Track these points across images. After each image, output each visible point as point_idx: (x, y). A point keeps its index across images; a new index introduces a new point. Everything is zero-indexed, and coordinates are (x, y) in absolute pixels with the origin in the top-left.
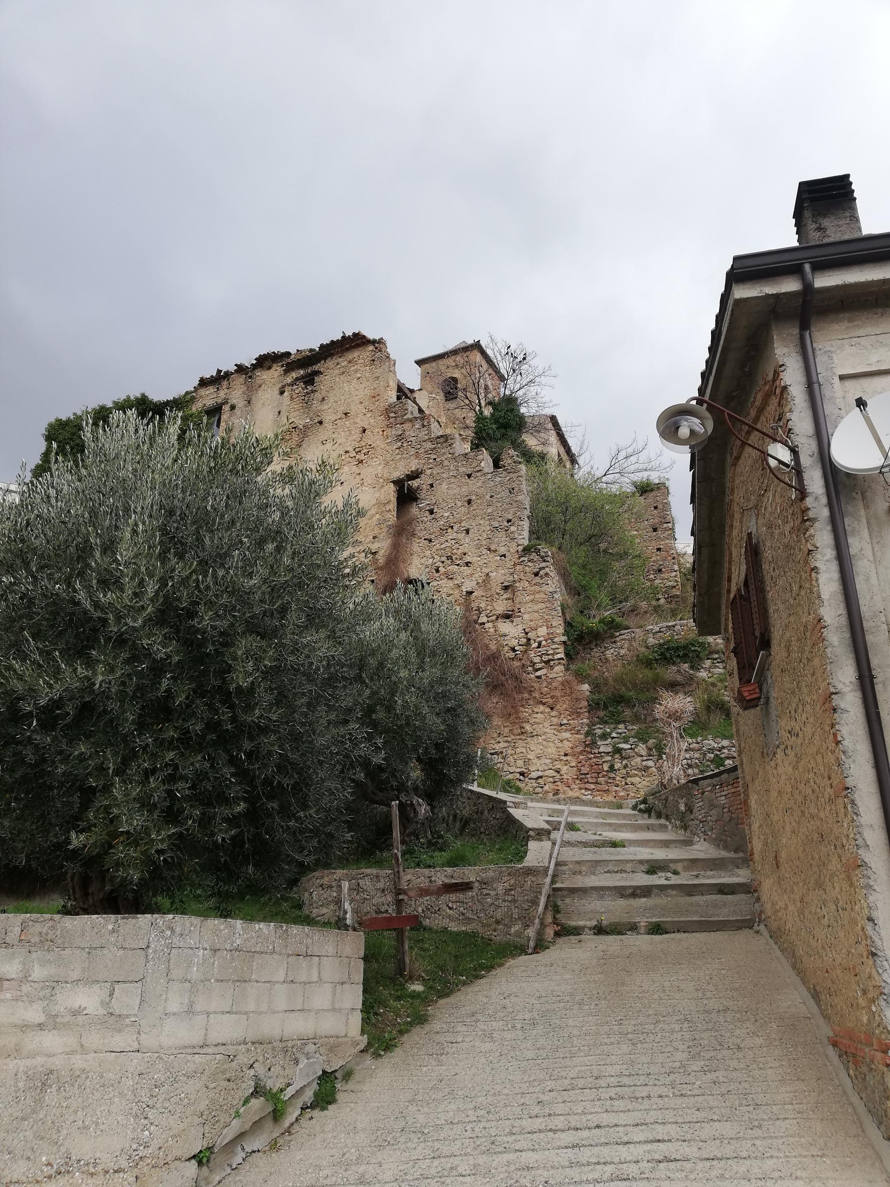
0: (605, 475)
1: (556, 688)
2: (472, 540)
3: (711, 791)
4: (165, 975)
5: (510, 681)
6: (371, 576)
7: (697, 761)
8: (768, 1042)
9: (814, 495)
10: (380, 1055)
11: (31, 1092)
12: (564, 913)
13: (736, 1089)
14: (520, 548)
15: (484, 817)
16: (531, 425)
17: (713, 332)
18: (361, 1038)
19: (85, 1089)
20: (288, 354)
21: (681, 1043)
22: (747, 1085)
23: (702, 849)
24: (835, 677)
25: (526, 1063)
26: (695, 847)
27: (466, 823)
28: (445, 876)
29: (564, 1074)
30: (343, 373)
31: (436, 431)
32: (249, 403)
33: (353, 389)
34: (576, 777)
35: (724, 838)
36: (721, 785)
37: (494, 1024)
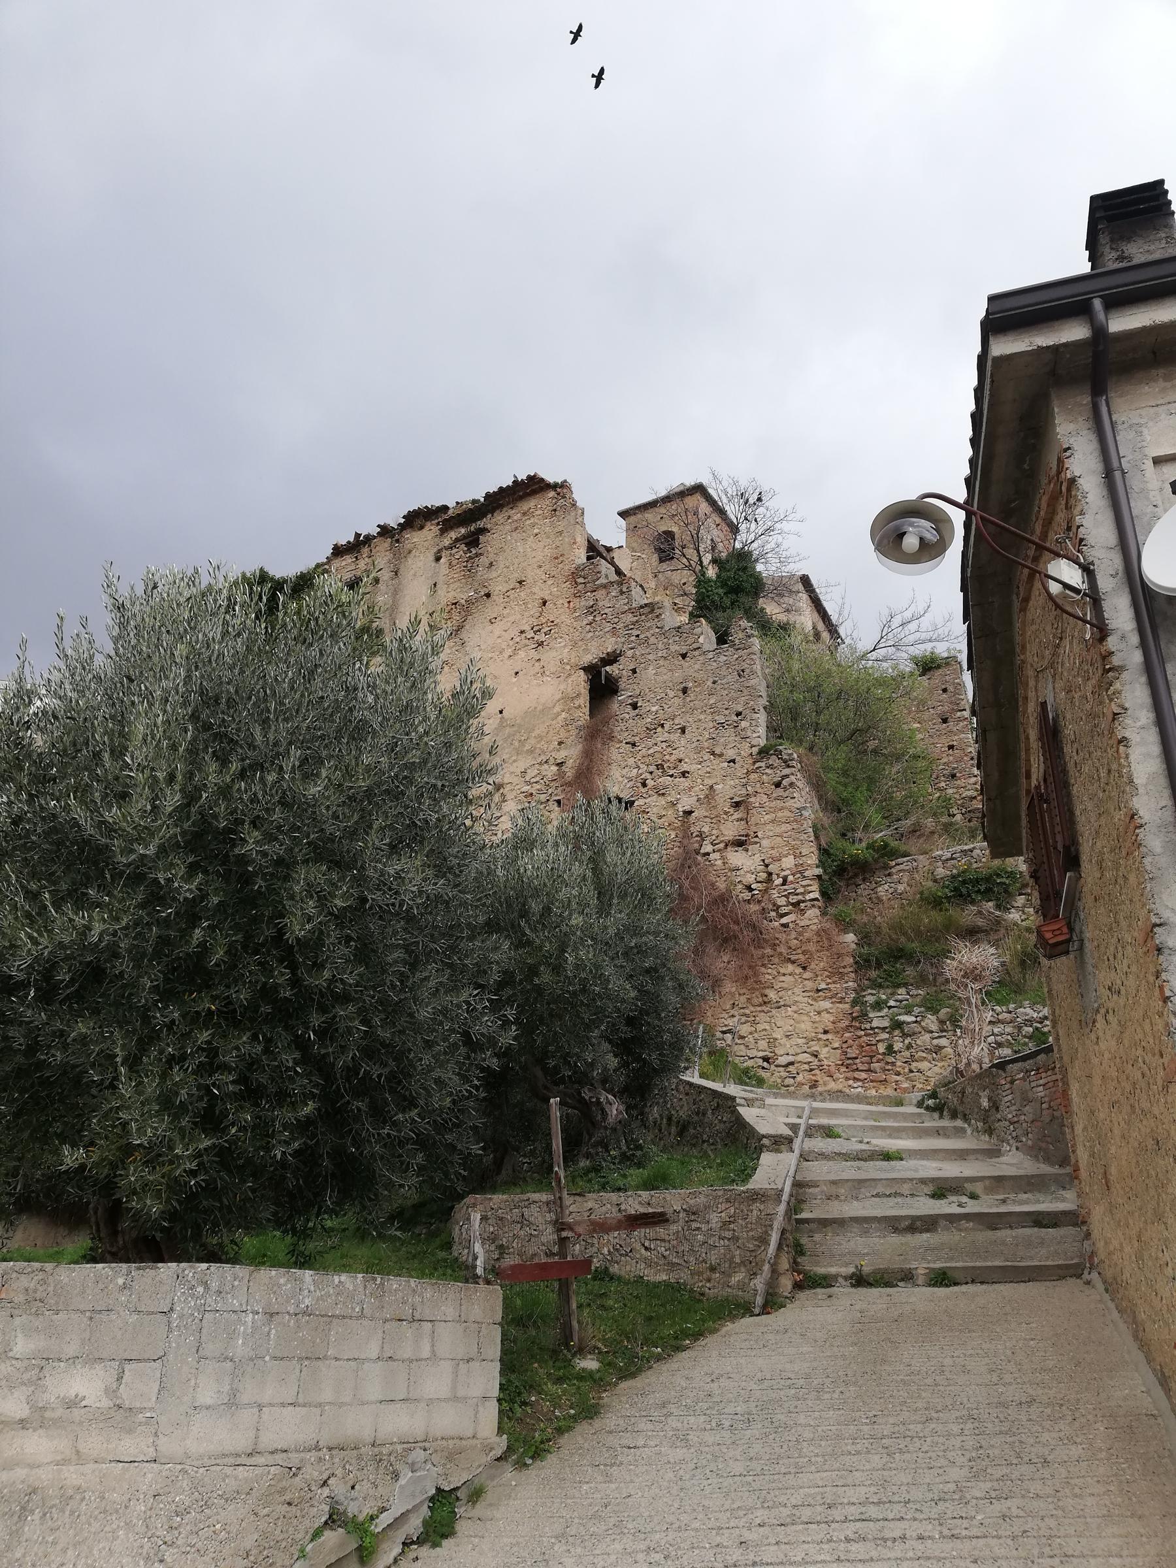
0: (874, 650)
1: (809, 940)
2: (690, 742)
3: (1023, 1079)
4: (194, 1350)
5: (745, 933)
6: (556, 795)
7: (1009, 1037)
8: (1090, 1453)
9: (1119, 633)
10: (525, 1465)
11: (6, 1521)
12: (810, 1255)
13: (1036, 1527)
14: (755, 750)
15: (706, 1120)
16: (772, 588)
17: (973, 416)
18: (497, 1439)
19: (79, 1516)
20: (445, 508)
21: (960, 1453)
22: (1052, 1523)
23: (1014, 1162)
24: (1158, 901)
25: (730, 1480)
26: (1003, 1159)
27: (683, 1128)
28: (640, 1203)
29: (782, 1499)
30: (516, 529)
31: (638, 597)
32: (396, 574)
33: (529, 550)
34: (840, 1063)
35: (1043, 1145)
36: (1038, 1069)
37: (692, 1419)
